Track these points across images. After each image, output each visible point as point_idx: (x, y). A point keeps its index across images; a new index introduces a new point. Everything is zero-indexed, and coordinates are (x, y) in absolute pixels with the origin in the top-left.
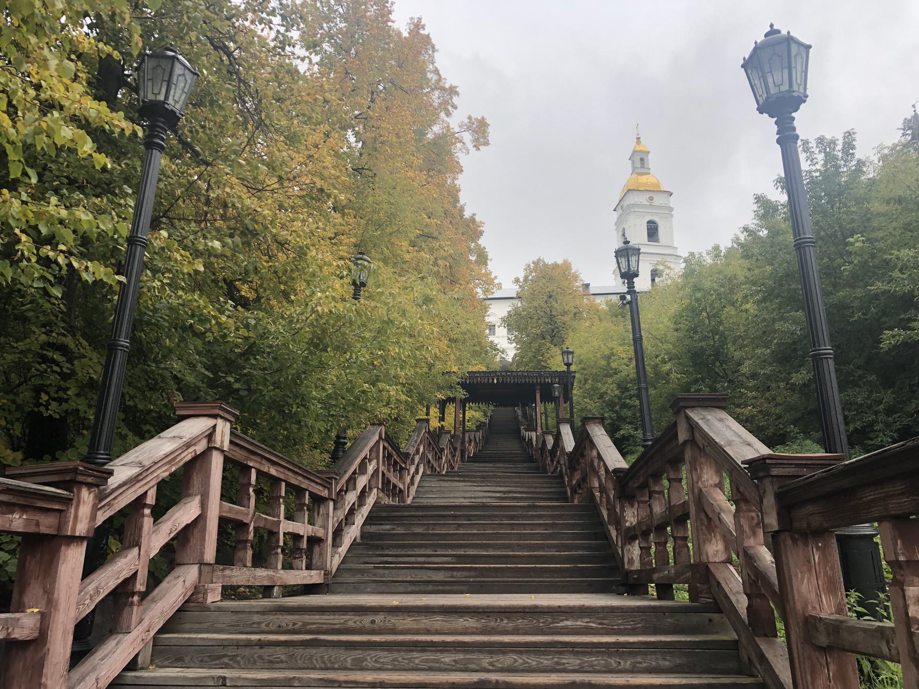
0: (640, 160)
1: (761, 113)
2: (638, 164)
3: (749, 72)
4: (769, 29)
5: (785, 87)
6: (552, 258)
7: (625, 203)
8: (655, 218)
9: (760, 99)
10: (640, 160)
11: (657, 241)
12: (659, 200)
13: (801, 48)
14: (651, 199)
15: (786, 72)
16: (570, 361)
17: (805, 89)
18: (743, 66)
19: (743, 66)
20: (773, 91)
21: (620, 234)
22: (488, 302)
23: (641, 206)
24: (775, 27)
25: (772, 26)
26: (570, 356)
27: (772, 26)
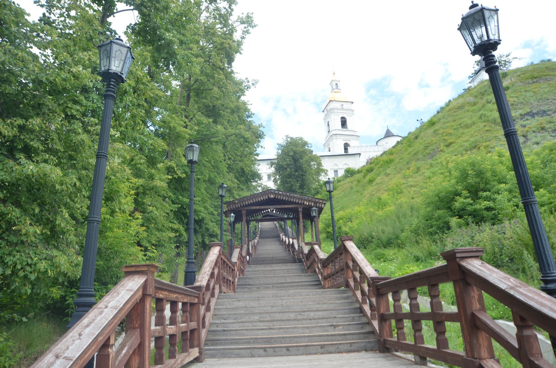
0: (336, 87)
1: (474, 55)
2: (334, 86)
3: (463, 32)
4: (471, 4)
5: (107, 68)
6: (295, 135)
7: (328, 108)
8: (345, 116)
9: (471, 47)
10: (336, 87)
11: (346, 128)
12: (346, 106)
13: (492, 12)
14: (342, 105)
15: (122, 63)
16: (332, 189)
17: (499, 37)
18: (458, 29)
19: (458, 29)
20: (478, 42)
21: (327, 124)
22: (321, 158)
23: (337, 109)
24: (475, 3)
25: (472, 2)
26: (331, 185)
27: (472, 2)
